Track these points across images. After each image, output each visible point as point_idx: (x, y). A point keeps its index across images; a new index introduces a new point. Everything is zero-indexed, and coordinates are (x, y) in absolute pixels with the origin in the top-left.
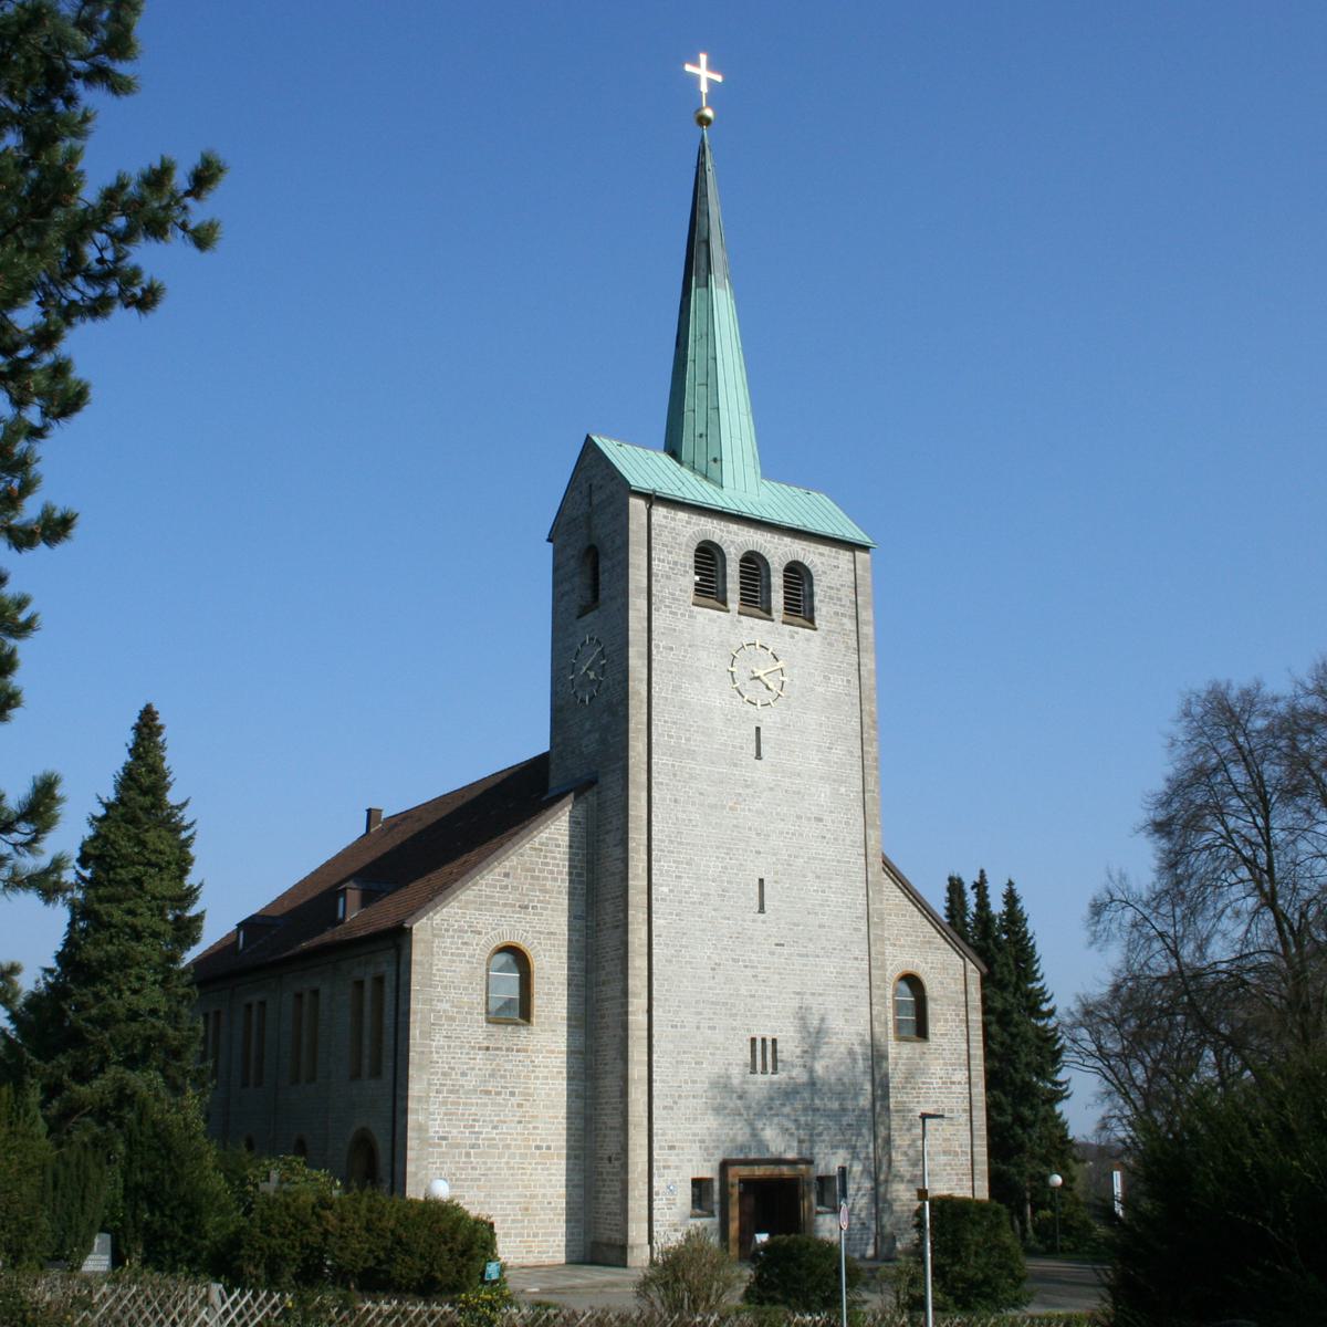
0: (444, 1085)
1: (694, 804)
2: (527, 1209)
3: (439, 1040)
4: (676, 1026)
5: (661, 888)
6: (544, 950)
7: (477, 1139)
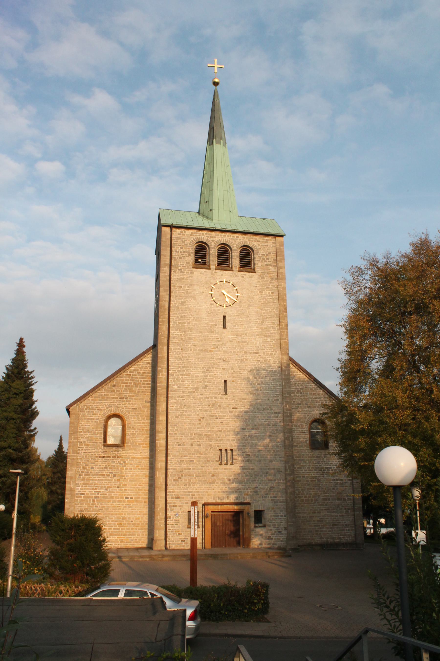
0: (83, 472)
1: (191, 350)
2: (121, 524)
3: (81, 454)
4: (180, 445)
5: (174, 387)
6: (132, 416)
7: (98, 494)
